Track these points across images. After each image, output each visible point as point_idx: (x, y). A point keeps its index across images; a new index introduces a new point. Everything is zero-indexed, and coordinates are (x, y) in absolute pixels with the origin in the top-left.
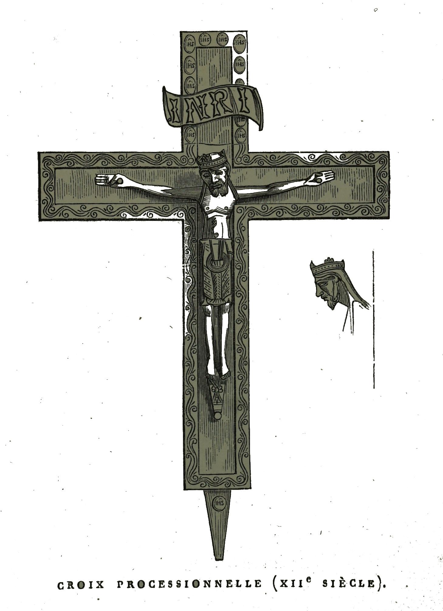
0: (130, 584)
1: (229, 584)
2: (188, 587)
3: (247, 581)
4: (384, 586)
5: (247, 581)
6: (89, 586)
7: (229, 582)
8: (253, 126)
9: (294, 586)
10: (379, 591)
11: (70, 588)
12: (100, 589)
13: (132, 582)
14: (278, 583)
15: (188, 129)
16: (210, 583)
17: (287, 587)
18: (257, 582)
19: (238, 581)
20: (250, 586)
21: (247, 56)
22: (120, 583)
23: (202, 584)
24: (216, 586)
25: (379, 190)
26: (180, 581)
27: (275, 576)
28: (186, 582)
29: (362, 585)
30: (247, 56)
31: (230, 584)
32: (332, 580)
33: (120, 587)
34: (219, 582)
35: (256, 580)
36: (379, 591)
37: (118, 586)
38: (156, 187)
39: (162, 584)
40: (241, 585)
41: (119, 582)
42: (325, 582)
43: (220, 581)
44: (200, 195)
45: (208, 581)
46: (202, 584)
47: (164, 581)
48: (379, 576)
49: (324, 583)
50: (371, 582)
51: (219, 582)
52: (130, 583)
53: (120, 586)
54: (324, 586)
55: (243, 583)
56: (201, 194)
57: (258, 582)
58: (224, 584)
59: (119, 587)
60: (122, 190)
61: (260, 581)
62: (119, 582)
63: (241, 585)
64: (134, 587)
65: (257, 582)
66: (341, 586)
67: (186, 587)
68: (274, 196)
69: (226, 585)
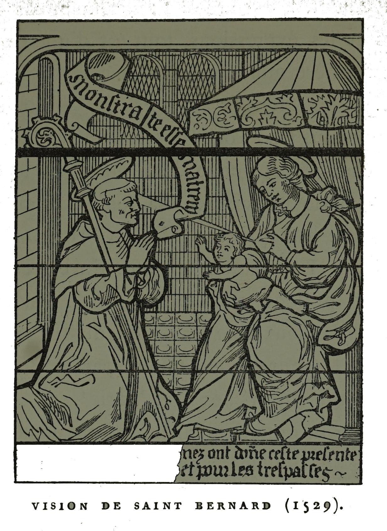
0: (147, 506)
4: (341, 508)
6: (44, 508)
7: (210, 504)
10: (334, 513)
12: (243, 510)
13: (223, 504)
14: (291, 505)
15: (50, 121)
16: (235, 505)
17: (150, 509)
18: (116, 504)
23: (78, 506)
24: (165, 508)
26: (138, 504)
27: (288, 499)
28: (62, 504)
31: (211, 506)
34: (233, 504)
36: (334, 513)
43: (234, 503)
44: (324, 158)
45: (234, 503)
46: (78, 506)
47: (119, 503)
48: (334, 498)
49: (135, 505)
50: (147, 506)
51: (233, 504)
52: (255, 504)
54: (135, 508)
56: (321, 156)
58: (205, 506)
61: (119, 503)
64: (224, 509)
66: (115, 508)
67: (62, 509)
68: (250, 158)
69: (114, 507)
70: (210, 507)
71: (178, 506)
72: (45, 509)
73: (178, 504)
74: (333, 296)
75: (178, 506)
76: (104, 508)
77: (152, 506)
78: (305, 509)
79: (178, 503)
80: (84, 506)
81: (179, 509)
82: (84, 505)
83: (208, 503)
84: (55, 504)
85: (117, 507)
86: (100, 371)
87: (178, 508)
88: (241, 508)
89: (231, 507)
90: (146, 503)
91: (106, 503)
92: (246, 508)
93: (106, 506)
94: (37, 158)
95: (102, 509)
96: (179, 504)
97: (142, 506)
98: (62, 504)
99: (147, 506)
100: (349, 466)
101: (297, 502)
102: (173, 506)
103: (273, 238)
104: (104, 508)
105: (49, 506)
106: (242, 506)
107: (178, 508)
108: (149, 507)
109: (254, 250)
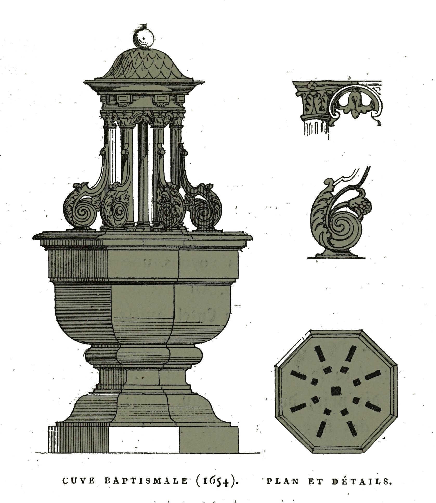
1: (311, 482)
2: (321, 484)
3: (175, 479)
4: (237, 483)
5: (175, 479)
8: (154, 123)
9: (142, 483)
11: (155, 483)
12: (116, 484)
14: (201, 481)
17: (119, 483)
18: (184, 480)
19: (277, 479)
20: (177, 483)
21: (152, 64)
22: (270, 480)
25: (80, 212)
26: (149, 479)
29: (176, 482)
30: (152, 64)
32: (376, 479)
33: (125, 483)
35: (123, 477)
37: (267, 482)
38: (329, 80)
39: (312, 481)
40: (178, 482)
41: (268, 479)
42: (311, 480)
43: (297, 479)
49: (147, 480)
53: (125, 482)
55: (179, 480)
57: (92, 479)
59: (268, 483)
60: (87, 242)
61: (93, 478)
62: (268, 479)
63: (178, 482)
65: (184, 480)
66: (90, 483)
70: (311, 483)
71: (320, 481)
72: (141, 483)
73: (320, 480)
74: (316, 124)
75: (320, 481)
76: (333, 484)
77: (367, 481)
78: (218, 484)
79: (353, 480)
80: (296, 481)
81: (321, 484)
82: (296, 481)
83: (310, 479)
84: (147, 482)
85: (311, 483)
86: (185, 385)
87: (320, 483)
88: (114, 483)
89: (294, 482)
90: (362, 479)
91: (336, 479)
92: (364, 484)
93: (335, 482)
94: (103, 245)
95: (332, 484)
96: (355, 480)
97: (87, 481)
98: (141, 479)
99: (363, 482)
100: (57, 448)
101: (206, 478)
102: (316, 482)
103: (162, 158)
104: (333, 484)
105: (144, 481)
106: (115, 481)
107: (320, 483)
108: (365, 483)
109: (115, 220)
